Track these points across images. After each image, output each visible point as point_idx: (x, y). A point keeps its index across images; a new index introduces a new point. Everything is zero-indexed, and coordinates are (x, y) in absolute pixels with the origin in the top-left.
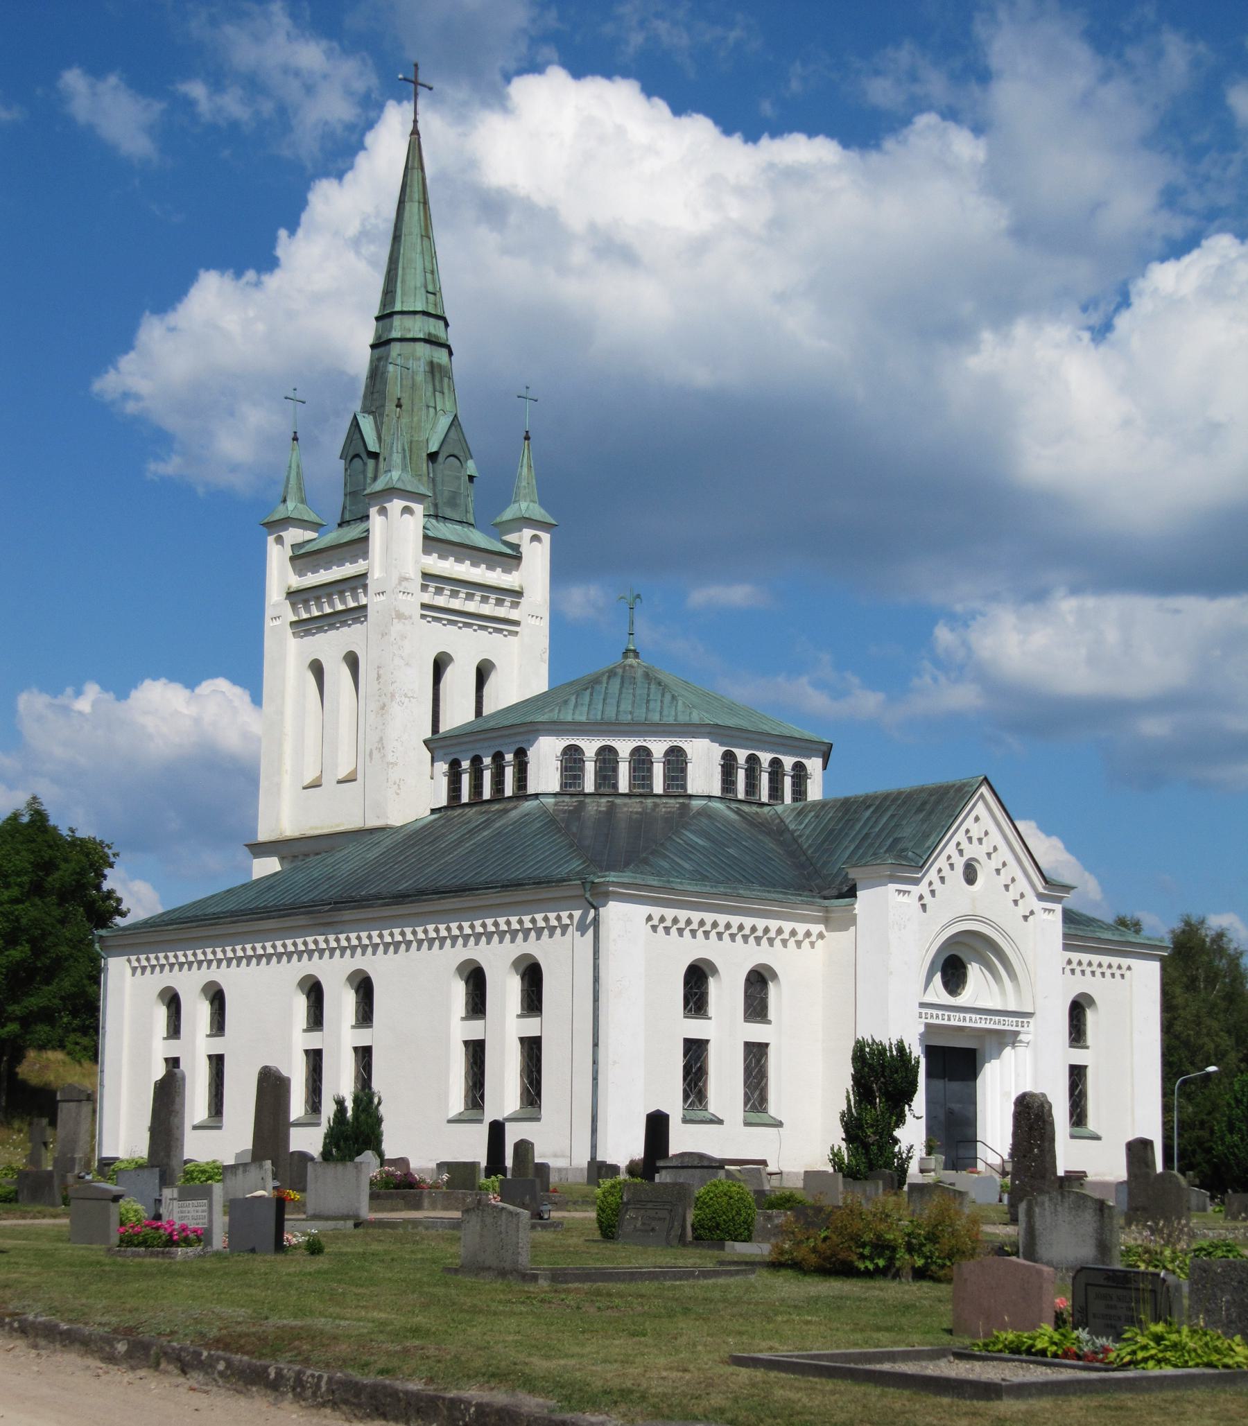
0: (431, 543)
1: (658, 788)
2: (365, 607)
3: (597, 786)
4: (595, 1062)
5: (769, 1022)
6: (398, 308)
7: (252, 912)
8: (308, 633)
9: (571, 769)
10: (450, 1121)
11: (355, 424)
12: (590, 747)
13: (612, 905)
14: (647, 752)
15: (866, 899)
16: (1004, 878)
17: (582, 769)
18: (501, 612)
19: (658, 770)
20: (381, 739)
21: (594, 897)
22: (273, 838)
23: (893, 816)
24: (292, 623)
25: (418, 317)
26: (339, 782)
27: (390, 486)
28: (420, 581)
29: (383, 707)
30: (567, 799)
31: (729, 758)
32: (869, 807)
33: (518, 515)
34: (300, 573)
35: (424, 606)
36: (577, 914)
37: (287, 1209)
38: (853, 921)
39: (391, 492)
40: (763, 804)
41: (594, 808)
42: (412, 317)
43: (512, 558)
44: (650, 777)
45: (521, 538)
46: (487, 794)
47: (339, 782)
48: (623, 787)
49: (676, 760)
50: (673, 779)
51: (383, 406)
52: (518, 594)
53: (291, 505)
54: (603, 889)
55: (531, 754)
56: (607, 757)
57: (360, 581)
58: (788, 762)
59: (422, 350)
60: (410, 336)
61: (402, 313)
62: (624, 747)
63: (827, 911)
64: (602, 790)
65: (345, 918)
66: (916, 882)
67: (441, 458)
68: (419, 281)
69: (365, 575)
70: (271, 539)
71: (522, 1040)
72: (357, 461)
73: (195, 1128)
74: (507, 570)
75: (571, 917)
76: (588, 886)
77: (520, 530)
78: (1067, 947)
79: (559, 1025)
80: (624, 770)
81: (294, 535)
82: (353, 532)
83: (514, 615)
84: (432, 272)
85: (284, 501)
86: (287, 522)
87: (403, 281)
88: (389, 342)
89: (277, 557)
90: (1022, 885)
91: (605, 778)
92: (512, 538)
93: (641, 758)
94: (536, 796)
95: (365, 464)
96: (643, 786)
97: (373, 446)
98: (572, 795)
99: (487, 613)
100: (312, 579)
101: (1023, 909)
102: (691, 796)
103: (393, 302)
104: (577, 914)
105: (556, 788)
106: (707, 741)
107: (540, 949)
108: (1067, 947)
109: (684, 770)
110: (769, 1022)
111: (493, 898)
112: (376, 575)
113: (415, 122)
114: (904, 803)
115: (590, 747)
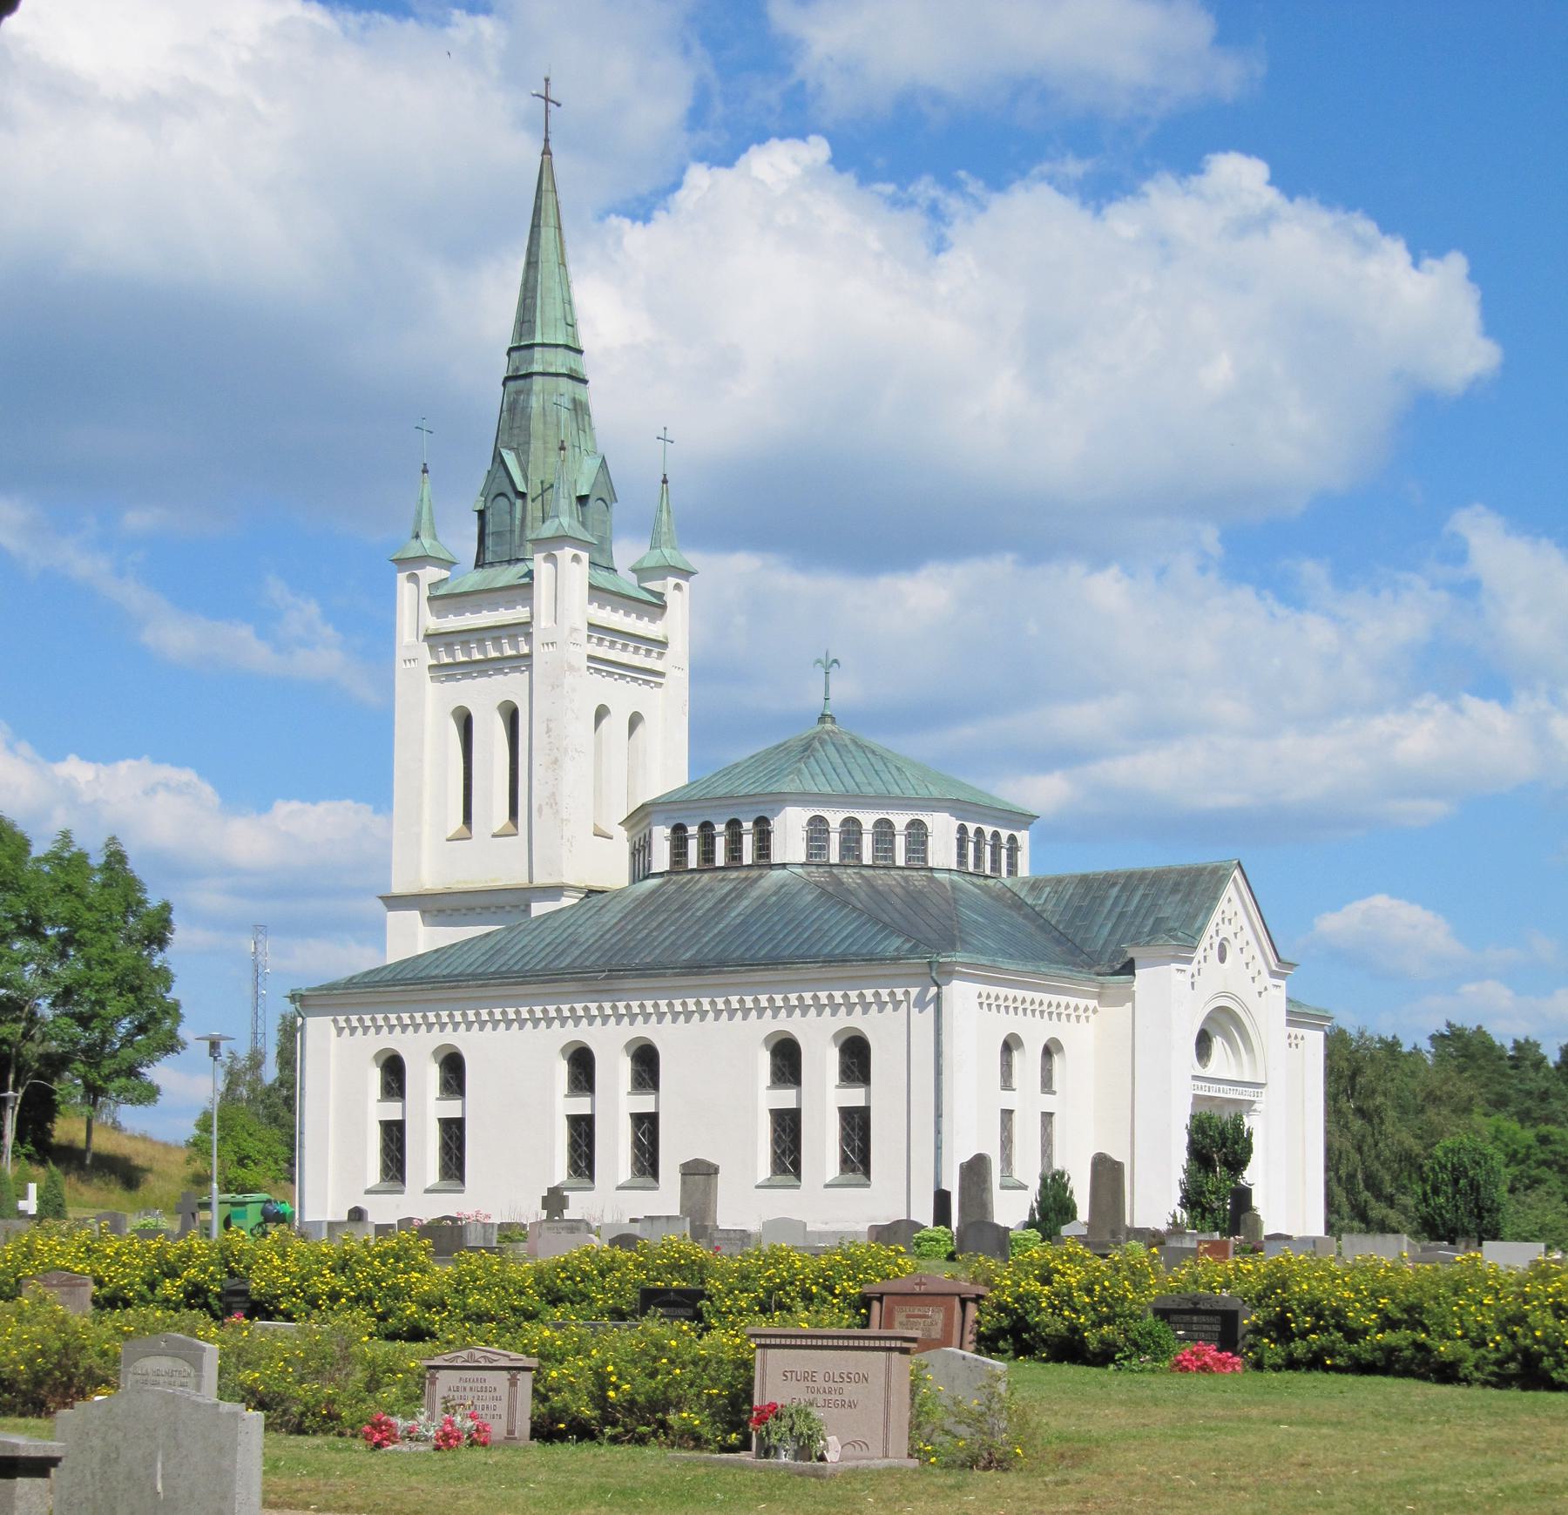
0: (597, 592)
1: (900, 860)
2: (529, 656)
3: (842, 857)
4: (938, 1132)
5: (1054, 1093)
6: (538, 340)
7: (475, 976)
8: (450, 678)
9: (817, 839)
10: (758, 1187)
11: (498, 459)
12: (835, 818)
13: (955, 983)
14: (889, 823)
15: (1143, 976)
16: (1246, 957)
17: (827, 840)
19: (900, 842)
21: (939, 975)
22: (415, 891)
23: (1145, 896)
24: (430, 667)
26: (494, 836)
28: (585, 631)
29: (556, 761)
30: (813, 869)
31: (962, 830)
32: (1114, 884)
33: (662, 562)
34: (439, 614)
35: (591, 658)
36: (914, 991)
38: (1131, 997)
39: (562, 540)
40: (987, 877)
43: (656, 606)
44: (892, 850)
45: (665, 586)
46: (693, 862)
47: (494, 836)
48: (867, 859)
49: (918, 832)
51: (528, 443)
52: (663, 644)
53: (426, 541)
54: (949, 968)
55: (776, 824)
56: (851, 829)
57: (523, 629)
58: (1005, 834)
59: (565, 385)
60: (552, 370)
61: (543, 345)
62: (868, 819)
64: (846, 862)
66: (1189, 961)
67: (591, 501)
68: (559, 315)
69: (528, 624)
70: (402, 577)
71: (841, 1109)
72: (502, 501)
73: (1025, 1188)
74: (652, 620)
75: (907, 993)
76: (935, 966)
78: (1290, 1023)
79: (883, 1097)
80: (867, 841)
81: (430, 574)
82: (508, 575)
83: (658, 666)
84: (570, 303)
85: (417, 536)
86: (424, 560)
88: (530, 375)
89: (409, 598)
90: (1260, 963)
91: (849, 849)
92: (655, 585)
93: (884, 830)
94: (784, 866)
95: (512, 505)
96: (885, 858)
97: (521, 488)
98: (818, 866)
100: (453, 623)
101: (1258, 987)
102: (932, 869)
103: (532, 332)
104: (914, 991)
106: (946, 815)
108: (1290, 1023)
110: (1054, 1093)
111: (814, 971)
112: (543, 623)
113: (547, 140)
114: (1152, 884)
115: (835, 818)
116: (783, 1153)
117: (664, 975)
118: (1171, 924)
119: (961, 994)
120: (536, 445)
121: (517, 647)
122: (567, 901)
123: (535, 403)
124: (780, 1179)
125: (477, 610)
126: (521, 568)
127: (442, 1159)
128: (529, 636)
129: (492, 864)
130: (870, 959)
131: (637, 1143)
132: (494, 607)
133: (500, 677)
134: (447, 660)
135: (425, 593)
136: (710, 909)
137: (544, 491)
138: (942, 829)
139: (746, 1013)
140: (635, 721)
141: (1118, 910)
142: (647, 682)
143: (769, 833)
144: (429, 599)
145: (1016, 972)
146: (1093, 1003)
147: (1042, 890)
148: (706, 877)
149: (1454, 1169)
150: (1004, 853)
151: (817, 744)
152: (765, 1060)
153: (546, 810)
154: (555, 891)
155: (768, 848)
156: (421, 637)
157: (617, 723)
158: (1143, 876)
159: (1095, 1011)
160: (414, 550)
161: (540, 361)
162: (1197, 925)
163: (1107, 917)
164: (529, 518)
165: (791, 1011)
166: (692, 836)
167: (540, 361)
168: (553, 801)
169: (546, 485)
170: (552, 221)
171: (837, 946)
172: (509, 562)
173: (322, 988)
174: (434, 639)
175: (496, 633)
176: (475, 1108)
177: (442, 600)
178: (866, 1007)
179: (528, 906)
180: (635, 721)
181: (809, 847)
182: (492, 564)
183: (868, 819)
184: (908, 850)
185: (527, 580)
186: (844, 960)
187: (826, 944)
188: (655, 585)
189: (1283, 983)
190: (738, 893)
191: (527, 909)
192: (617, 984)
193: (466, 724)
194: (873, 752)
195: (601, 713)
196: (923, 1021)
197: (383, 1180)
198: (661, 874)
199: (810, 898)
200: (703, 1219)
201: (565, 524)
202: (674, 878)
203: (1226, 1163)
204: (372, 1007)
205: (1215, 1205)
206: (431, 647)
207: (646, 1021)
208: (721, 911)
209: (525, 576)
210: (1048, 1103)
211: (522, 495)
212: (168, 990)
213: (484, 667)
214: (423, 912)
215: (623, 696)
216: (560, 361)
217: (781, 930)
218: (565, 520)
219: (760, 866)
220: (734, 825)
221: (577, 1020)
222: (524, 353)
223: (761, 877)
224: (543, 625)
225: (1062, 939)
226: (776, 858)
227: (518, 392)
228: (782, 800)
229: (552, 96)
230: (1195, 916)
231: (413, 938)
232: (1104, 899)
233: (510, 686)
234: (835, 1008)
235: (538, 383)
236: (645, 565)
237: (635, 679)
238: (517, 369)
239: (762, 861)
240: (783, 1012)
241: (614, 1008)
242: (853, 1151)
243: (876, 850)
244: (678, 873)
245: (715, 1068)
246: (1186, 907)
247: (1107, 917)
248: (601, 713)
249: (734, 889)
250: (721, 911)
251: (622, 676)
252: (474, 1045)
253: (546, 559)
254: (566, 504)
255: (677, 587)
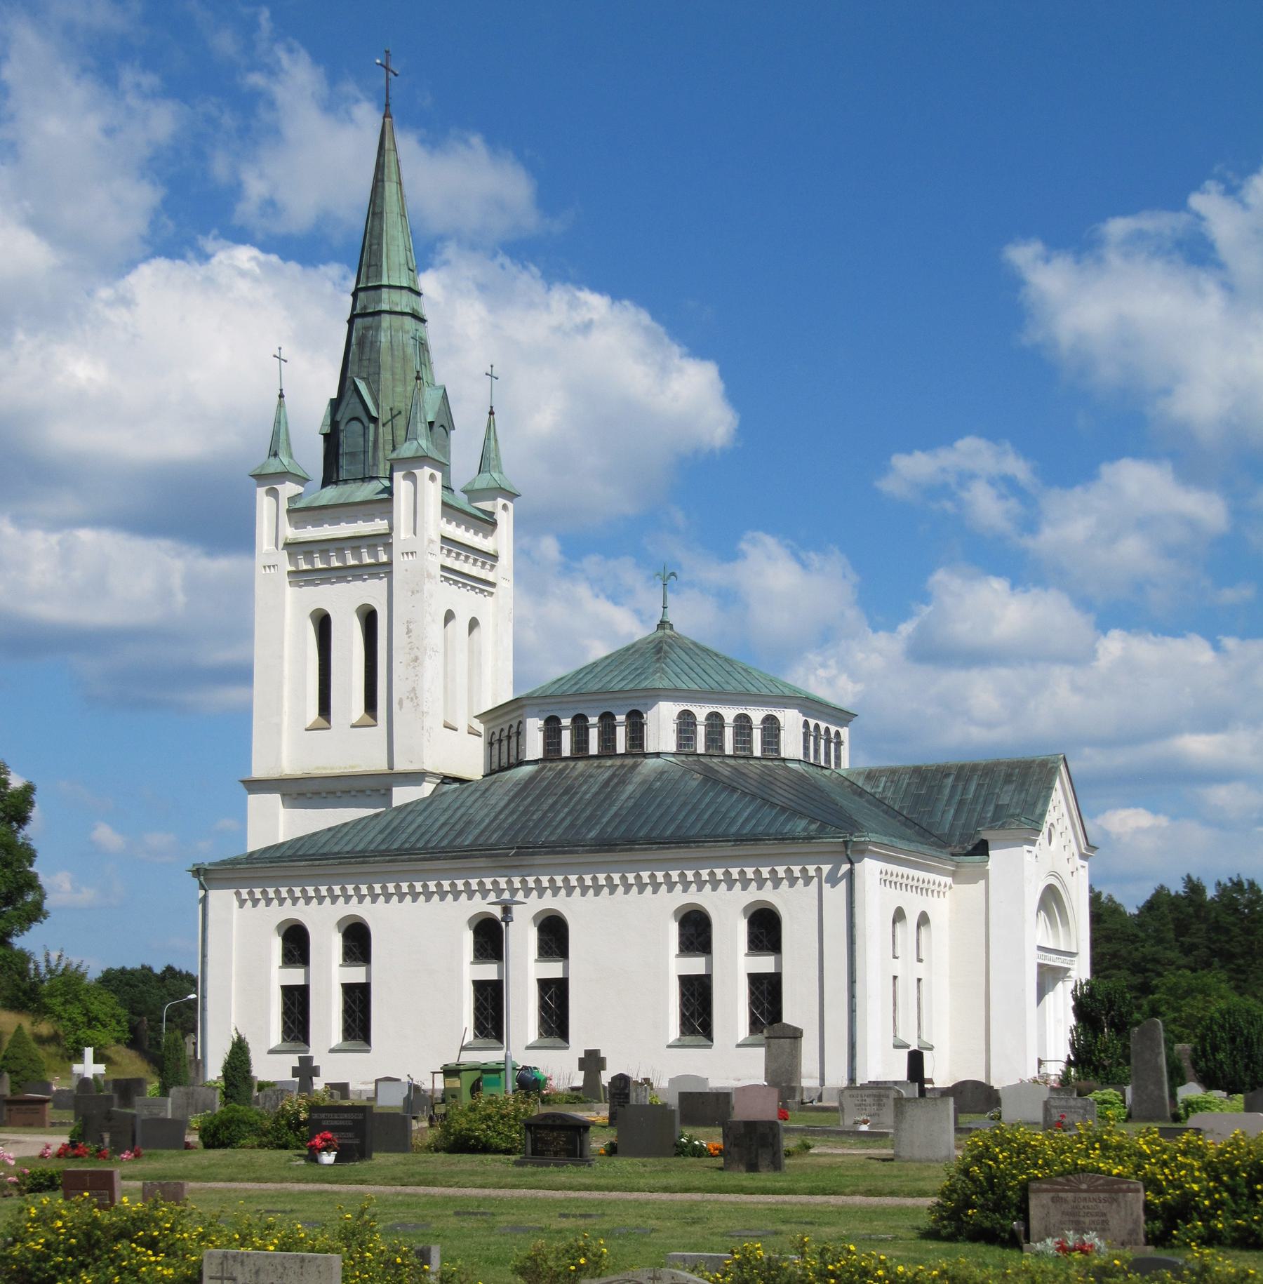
1: (757, 752)
3: (707, 747)
6: (385, 282)
9: (685, 731)
12: (701, 712)
15: (997, 857)
17: (694, 732)
18: (483, 574)
19: (757, 735)
20: (414, 689)
21: (852, 853)
23: (980, 786)
24: (289, 573)
25: (404, 292)
26: (353, 726)
27: (420, 453)
28: (439, 544)
29: (416, 659)
30: (683, 758)
31: (806, 724)
32: (947, 775)
33: (493, 484)
34: (297, 525)
35: (444, 568)
36: (826, 868)
37: (162, 1115)
38: (985, 875)
41: (754, 768)
42: (398, 291)
43: (487, 523)
44: (750, 742)
45: (495, 506)
47: (353, 726)
49: (772, 727)
50: (769, 743)
52: (494, 557)
54: (862, 847)
55: (650, 717)
56: (715, 722)
57: (384, 539)
58: (833, 729)
59: (409, 322)
60: (398, 309)
61: (390, 287)
62: (729, 714)
63: (957, 867)
64: (711, 752)
65: (525, 863)
68: (403, 261)
72: (356, 426)
74: (485, 536)
75: (819, 870)
76: (850, 845)
77: (495, 499)
80: (729, 733)
81: (288, 489)
82: (366, 491)
83: (490, 577)
85: (276, 455)
86: (284, 476)
87: (387, 257)
92: (486, 505)
93: (743, 724)
94: (658, 755)
95: (365, 428)
96: (744, 749)
97: (374, 413)
99: (466, 571)
102: (784, 760)
104: (826, 868)
105: (673, 749)
107: (778, 898)
109: (777, 736)
111: (728, 849)
112: (402, 534)
113: (387, 105)
115: (701, 712)
116: (692, 1015)
117: (576, 852)
118: (1012, 811)
119: (870, 870)
120: (385, 376)
121: (376, 556)
122: (427, 789)
123: (384, 338)
124: (548, 1041)
125: (335, 521)
126: (376, 486)
127: (345, 1021)
128: (389, 547)
129: (351, 749)
130: (782, 839)
131: (543, 1007)
132: (352, 519)
133: (359, 583)
134: (305, 567)
135: (284, 505)
136: (597, 794)
137: (393, 417)
138: (791, 721)
139: (321, 900)
140: (473, 624)
141: (957, 798)
142: (482, 591)
143: (642, 725)
144: (289, 511)
145: (907, 852)
146: (949, 880)
147: (878, 779)
148: (581, 765)
149: (1231, 1029)
150: (832, 745)
151: (666, 647)
152: (277, 944)
153: (406, 703)
154: (416, 777)
155: (642, 738)
156: (281, 545)
157: (461, 623)
158: (974, 768)
159: (950, 888)
160: (274, 466)
161: (388, 300)
162: (1038, 811)
163: (948, 803)
164: (381, 441)
165: (701, 885)
166: (566, 728)
167: (388, 300)
168: (414, 694)
169: (395, 412)
170: (394, 177)
171: (743, 825)
172: (363, 480)
173: (223, 862)
174: (293, 548)
175: (356, 543)
176: (383, 972)
177: (300, 513)
178: (777, 882)
179: (389, 791)
180: (473, 624)
181: (679, 738)
182: (346, 481)
183: (729, 714)
184: (763, 743)
185: (385, 496)
186: (755, 839)
187: (730, 825)
188: (486, 505)
189: (1086, 864)
190: (620, 779)
191: (388, 794)
192: (527, 860)
193: (323, 624)
194: (716, 655)
195: (449, 616)
196: (836, 896)
197: (284, 1040)
198: (536, 762)
199: (695, 784)
200: (791, 1080)
201: (424, 446)
202: (549, 765)
203: (1112, 1025)
204: (276, 881)
205: (1106, 1063)
206: (289, 554)
207: (555, 895)
208: (608, 796)
209: (382, 492)
210: (920, 970)
211: (374, 420)
212: (31, 865)
213: (358, 572)
214: (283, 795)
215: (465, 602)
216: (403, 302)
217: (679, 811)
218: (423, 443)
219: (634, 755)
220: (607, 720)
221: (701, 885)
222: (372, 293)
223: (635, 766)
224: (403, 536)
225: (909, 822)
226: (650, 746)
227: (367, 328)
228: (656, 695)
229: (392, 66)
230: (1034, 805)
231: (274, 824)
232: (940, 788)
233: (371, 592)
234: (671, 886)
235: (386, 320)
236: (477, 486)
237: (473, 588)
238: (365, 307)
239: (635, 751)
240: (694, 887)
241: (524, 882)
242: (762, 1014)
243: (736, 742)
244: (552, 760)
245: (624, 940)
246: (1023, 796)
247: (948, 803)
248: (449, 616)
249: (614, 775)
250: (608, 796)
251: (465, 585)
252: (381, 917)
253: (405, 477)
254: (422, 428)
255: (505, 507)
